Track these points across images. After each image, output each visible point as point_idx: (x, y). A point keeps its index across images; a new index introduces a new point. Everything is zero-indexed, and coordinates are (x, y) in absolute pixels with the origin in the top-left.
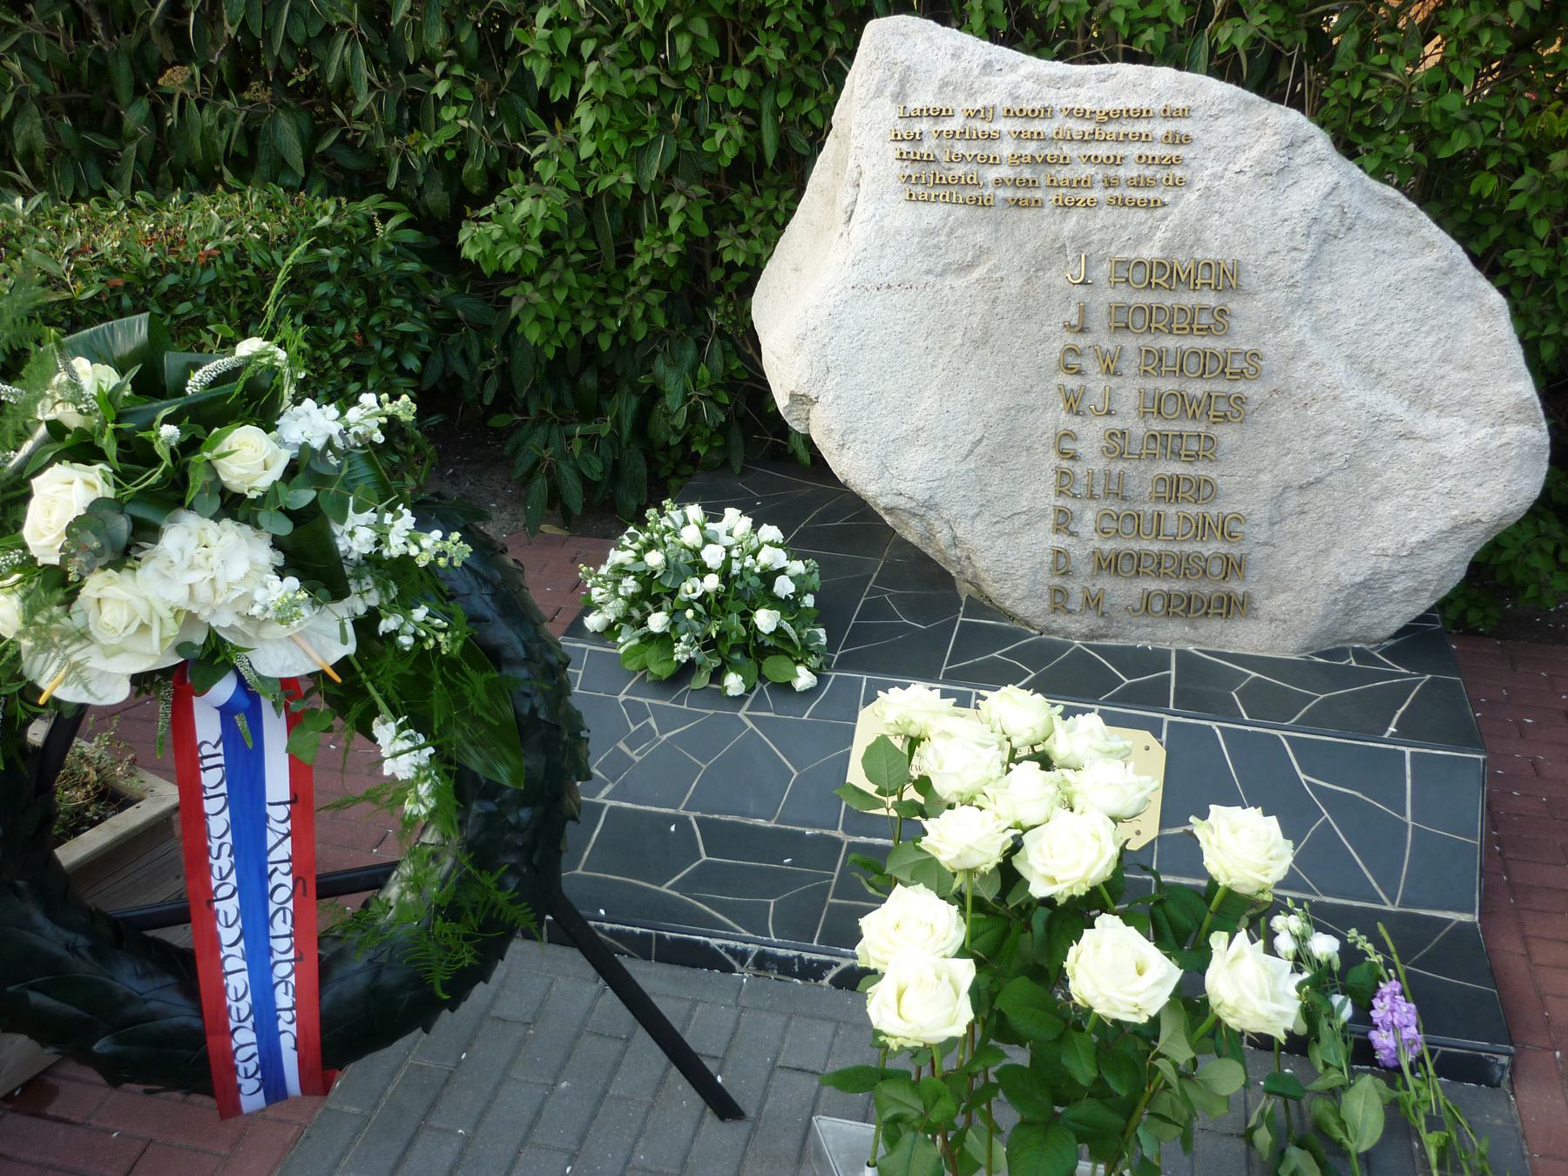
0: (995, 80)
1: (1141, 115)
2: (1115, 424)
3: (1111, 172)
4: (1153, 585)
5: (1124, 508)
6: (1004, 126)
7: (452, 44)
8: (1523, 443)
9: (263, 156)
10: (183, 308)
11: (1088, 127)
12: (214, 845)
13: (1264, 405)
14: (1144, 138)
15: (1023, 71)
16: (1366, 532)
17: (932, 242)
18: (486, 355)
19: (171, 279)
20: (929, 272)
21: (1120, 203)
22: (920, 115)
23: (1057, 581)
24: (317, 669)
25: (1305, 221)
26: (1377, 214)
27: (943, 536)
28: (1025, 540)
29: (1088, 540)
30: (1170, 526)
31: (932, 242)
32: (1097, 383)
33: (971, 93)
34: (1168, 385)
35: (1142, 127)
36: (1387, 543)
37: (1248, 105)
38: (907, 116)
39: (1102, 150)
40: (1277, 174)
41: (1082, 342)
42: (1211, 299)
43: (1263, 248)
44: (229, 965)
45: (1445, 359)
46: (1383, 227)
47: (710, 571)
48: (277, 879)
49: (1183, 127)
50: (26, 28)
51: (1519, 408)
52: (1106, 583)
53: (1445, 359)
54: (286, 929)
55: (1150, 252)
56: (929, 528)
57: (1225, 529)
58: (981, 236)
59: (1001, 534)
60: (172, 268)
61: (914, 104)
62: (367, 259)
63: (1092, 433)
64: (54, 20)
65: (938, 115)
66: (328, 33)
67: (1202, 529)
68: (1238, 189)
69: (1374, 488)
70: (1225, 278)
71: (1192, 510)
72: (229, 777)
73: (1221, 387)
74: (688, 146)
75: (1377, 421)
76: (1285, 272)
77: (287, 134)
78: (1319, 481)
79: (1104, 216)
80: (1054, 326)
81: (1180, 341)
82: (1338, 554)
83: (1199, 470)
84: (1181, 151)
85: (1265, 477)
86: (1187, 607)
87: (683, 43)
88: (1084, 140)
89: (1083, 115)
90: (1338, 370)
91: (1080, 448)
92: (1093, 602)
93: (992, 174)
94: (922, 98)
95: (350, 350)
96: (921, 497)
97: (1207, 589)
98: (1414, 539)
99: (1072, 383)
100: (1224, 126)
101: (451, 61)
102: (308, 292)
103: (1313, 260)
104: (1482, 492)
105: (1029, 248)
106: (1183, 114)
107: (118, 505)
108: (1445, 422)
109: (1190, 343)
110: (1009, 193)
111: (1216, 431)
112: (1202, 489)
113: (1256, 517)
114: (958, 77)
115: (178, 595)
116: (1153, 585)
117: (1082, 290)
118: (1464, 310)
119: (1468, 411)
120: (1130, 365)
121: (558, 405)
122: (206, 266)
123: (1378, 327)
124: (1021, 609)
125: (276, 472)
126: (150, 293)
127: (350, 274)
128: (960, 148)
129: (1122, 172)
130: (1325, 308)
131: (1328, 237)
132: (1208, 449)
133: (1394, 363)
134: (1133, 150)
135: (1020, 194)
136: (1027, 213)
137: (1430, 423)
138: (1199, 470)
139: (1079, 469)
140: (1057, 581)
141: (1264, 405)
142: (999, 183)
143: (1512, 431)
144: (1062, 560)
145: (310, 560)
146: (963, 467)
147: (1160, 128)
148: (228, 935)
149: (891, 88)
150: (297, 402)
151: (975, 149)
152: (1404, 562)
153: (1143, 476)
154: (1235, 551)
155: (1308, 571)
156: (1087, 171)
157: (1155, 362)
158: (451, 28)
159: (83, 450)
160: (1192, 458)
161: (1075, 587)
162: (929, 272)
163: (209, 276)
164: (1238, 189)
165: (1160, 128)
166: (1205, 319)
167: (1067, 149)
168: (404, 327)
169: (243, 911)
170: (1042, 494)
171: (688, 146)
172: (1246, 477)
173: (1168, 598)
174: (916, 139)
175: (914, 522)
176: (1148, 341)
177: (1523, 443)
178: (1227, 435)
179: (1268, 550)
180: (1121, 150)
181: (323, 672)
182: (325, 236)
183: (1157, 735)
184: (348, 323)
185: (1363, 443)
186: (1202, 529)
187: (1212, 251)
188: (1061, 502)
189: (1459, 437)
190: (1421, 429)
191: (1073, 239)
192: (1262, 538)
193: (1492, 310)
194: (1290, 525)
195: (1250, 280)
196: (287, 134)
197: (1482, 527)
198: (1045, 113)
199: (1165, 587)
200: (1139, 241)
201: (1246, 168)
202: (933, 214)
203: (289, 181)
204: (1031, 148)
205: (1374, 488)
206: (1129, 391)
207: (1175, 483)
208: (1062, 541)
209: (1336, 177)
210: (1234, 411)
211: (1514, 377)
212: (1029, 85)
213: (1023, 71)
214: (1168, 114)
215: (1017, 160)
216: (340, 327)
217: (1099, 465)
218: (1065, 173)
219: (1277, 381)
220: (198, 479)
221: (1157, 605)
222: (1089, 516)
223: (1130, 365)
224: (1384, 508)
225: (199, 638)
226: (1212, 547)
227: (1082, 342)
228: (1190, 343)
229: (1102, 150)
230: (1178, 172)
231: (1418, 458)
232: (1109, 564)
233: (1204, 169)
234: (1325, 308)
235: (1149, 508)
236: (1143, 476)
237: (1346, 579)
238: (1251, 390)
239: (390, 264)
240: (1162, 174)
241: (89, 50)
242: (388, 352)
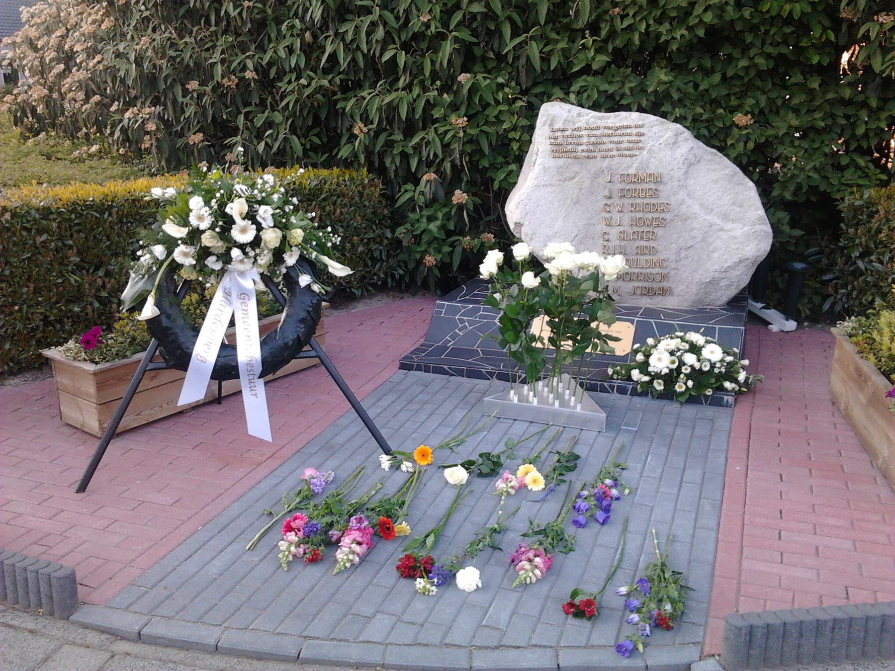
1: (627, 127)
2: (621, 229)
3: (619, 146)
4: (636, 284)
11: (611, 132)
16: (709, 264)
30: (643, 263)
32: (616, 216)
34: (640, 215)
35: (628, 131)
39: (615, 139)
42: (652, 186)
45: (734, 204)
49: (642, 130)
51: (760, 219)
53: (734, 204)
55: (632, 171)
57: (661, 264)
63: (614, 232)
65: (563, 130)
70: (657, 179)
73: (656, 215)
83: (651, 244)
84: (641, 138)
85: (673, 245)
89: (609, 128)
90: (696, 208)
93: (580, 148)
97: (655, 285)
103: (686, 172)
104: (747, 249)
106: (641, 126)
110: (586, 154)
116: (636, 284)
131: (691, 165)
134: (626, 138)
136: (592, 160)
137: (729, 226)
138: (651, 244)
142: (583, 151)
147: (634, 131)
151: (575, 140)
165: (634, 131)
174: (556, 138)
176: (631, 201)
178: (659, 231)
180: (621, 139)
185: (706, 233)
189: (738, 230)
195: (665, 179)
198: (598, 128)
200: (629, 167)
202: (561, 162)
204: (593, 139)
205: (711, 248)
206: (627, 218)
210: (661, 223)
214: (636, 127)
218: (604, 147)
221: (639, 292)
227: (609, 202)
229: (615, 139)
230: (640, 145)
238: (668, 216)
240: (635, 146)
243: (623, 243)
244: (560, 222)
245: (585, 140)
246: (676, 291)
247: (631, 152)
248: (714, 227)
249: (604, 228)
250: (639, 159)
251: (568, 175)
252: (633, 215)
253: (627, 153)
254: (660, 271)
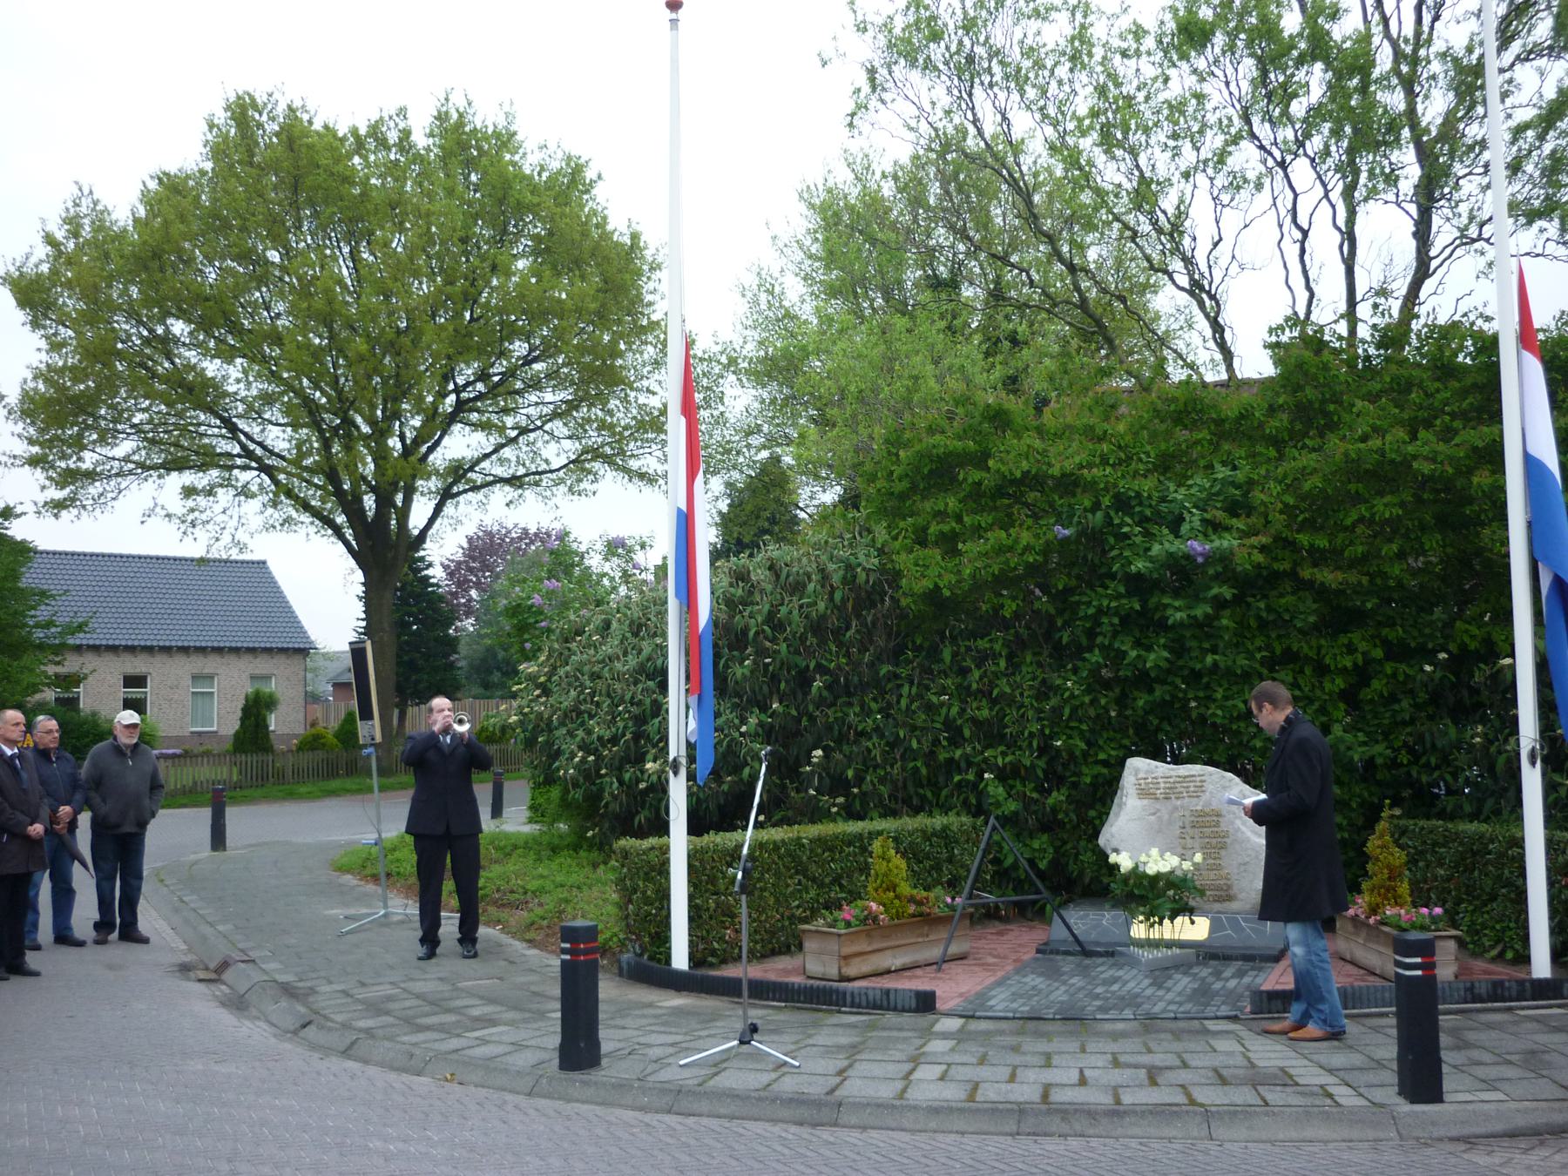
32: (1189, 841)
94: (1141, 775)
178: (1223, 852)
246: (1241, 896)
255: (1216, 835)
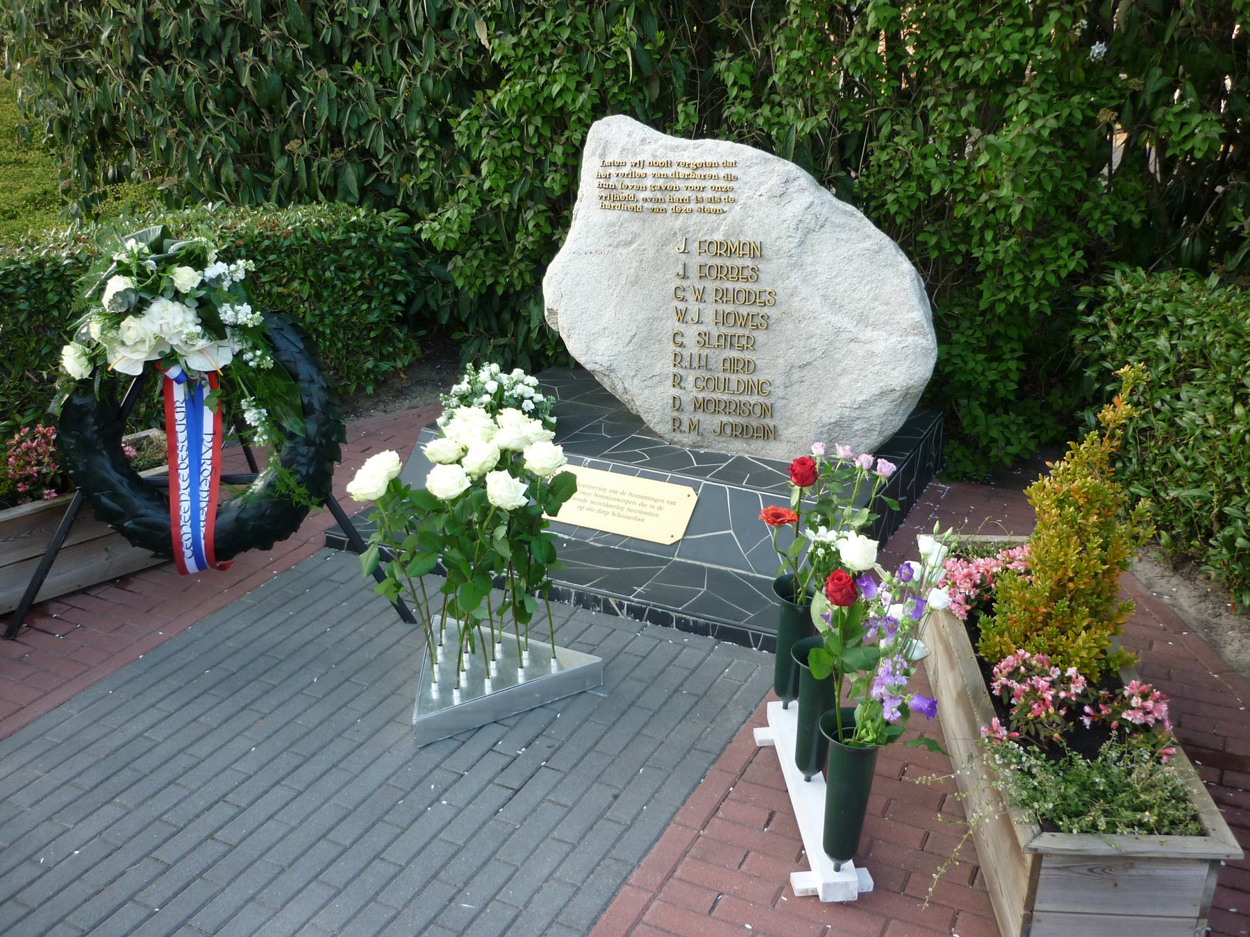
0: (646, 147)
2: (702, 328)
3: (699, 195)
4: (725, 419)
5: (708, 375)
6: (649, 171)
7: (425, 129)
8: (916, 346)
9: (340, 187)
10: (272, 257)
11: (687, 171)
12: (180, 445)
13: (779, 320)
14: (716, 178)
15: (660, 143)
16: (835, 394)
17: (611, 230)
18: (445, 296)
19: (266, 243)
20: (610, 245)
21: (703, 211)
22: (612, 164)
23: (675, 414)
24: (213, 369)
25: (795, 222)
26: (840, 220)
27: (620, 388)
28: (659, 390)
29: (690, 392)
30: (733, 386)
31: (611, 230)
32: (693, 307)
33: (635, 154)
34: (729, 308)
35: (713, 172)
36: (847, 400)
37: (766, 160)
38: (604, 165)
39: (694, 183)
40: (781, 196)
41: (685, 283)
42: (748, 262)
43: (774, 236)
44: (183, 498)
45: (875, 299)
46: (843, 227)
47: (487, 392)
48: (205, 466)
49: (733, 171)
50: (229, 119)
51: (915, 327)
52: (700, 416)
53: (875, 299)
54: (207, 488)
55: (718, 237)
56: (613, 383)
57: (760, 388)
58: (635, 227)
59: (647, 387)
60: (268, 237)
61: (609, 160)
62: (376, 240)
64: (243, 116)
66: (369, 123)
67: (749, 388)
68: (760, 204)
69: (839, 369)
70: (756, 251)
71: (745, 377)
72: (187, 417)
73: (754, 310)
74: (538, 183)
75: (838, 332)
76: (786, 249)
77: (351, 176)
78: (809, 364)
79: (696, 217)
80: (671, 275)
81: (732, 284)
82: (821, 406)
83: (746, 355)
84: (732, 184)
85: (781, 361)
86: (743, 432)
87: (531, 129)
88: (687, 178)
90: (815, 303)
91: (685, 341)
92: (694, 427)
93: (641, 195)
95: (362, 287)
96: (606, 364)
97: (754, 423)
98: (861, 398)
99: (681, 306)
100: (753, 171)
101: (424, 138)
102: (340, 255)
103: (801, 243)
104: (895, 373)
105: (659, 234)
106: (735, 164)
107: (135, 291)
108: (875, 334)
109: (740, 285)
110: (649, 205)
111: (755, 333)
112: (748, 366)
113: (777, 383)
114: (629, 146)
115: (156, 329)
116: (725, 419)
117: (684, 256)
118: (887, 272)
119: (888, 328)
120: (710, 296)
121: (488, 329)
122: (285, 238)
123: (839, 279)
124: (657, 429)
125: (195, 285)
126: (256, 249)
127: (365, 246)
128: (627, 182)
129: (705, 195)
130: (809, 269)
131: (809, 231)
132: (751, 344)
133: (847, 300)
134: (709, 183)
135: (656, 206)
136: (659, 216)
137: (869, 334)
138: (746, 355)
139: (686, 353)
140: (675, 414)
141: (779, 320)
143: (911, 339)
144: (677, 402)
145: (213, 327)
146: (627, 349)
147: (722, 172)
148: (183, 485)
149: (599, 151)
150: (215, 262)
151: (634, 182)
152: (858, 412)
153: (718, 357)
154: (768, 402)
155: (806, 415)
156: (687, 194)
157: (721, 295)
158: (425, 121)
159: (124, 270)
160: (742, 348)
161: (685, 418)
162: (610, 245)
163: (287, 243)
164: (760, 204)
165: (722, 172)
166: (747, 273)
167: (678, 183)
168: (396, 277)
169: (190, 476)
170: (666, 366)
171: (538, 183)
172: (772, 359)
173: (734, 427)
175: (605, 379)
176: (718, 284)
177: (916, 346)
178: (760, 336)
179: (784, 402)
180: (703, 183)
181: (215, 372)
182: (355, 227)
183: (696, 490)
184: (363, 272)
185: (831, 343)
186: (749, 388)
187: (747, 237)
188: (676, 370)
189: (882, 342)
190: (861, 337)
191: (680, 229)
192: (781, 395)
193: (902, 273)
194: (796, 388)
195: (767, 252)
196: (351, 176)
197: (898, 394)
198: (669, 164)
199: (731, 420)
200: (713, 231)
201: (764, 192)
202: (612, 215)
203: (352, 201)
204: (661, 182)
205: (839, 369)
207: (735, 362)
208: (676, 392)
209: (811, 199)
210: (764, 323)
211: (912, 309)
212: (662, 150)
213: (660, 143)
214: (726, 165)
215: (654, 188)
216: (358, 275)
217: (695, 350)
218: (677, 195)
219: (784, 308)
220: (164, 284)
221: (728, 430)
222: (691, 379)
223: (710, 296)
224: (844, 381)
225: (168, 351)
226: (754, 399)
227: (685, 283)
228: (740, 285)
229: (694, 183)
230: (731, 195)
231: (860, 353)
232: (701, 405)
233: (744, 193)
234: (809, 269)
235: (722, 376)
236: (718, 357)
237: (825, 420)
239: (389, 243)
241: (259, 130)
242: (387, 290)
243: (704, 352)
244: (609, 314)
245: (649, 182)
247: (718, 207)
248: (843, 335)
249: (673, 324)
250: (729, 219)
251: (622, 238)
252: (722, 307)
253: (712, 206)
254: (761, 399)
255: (751, 298)
